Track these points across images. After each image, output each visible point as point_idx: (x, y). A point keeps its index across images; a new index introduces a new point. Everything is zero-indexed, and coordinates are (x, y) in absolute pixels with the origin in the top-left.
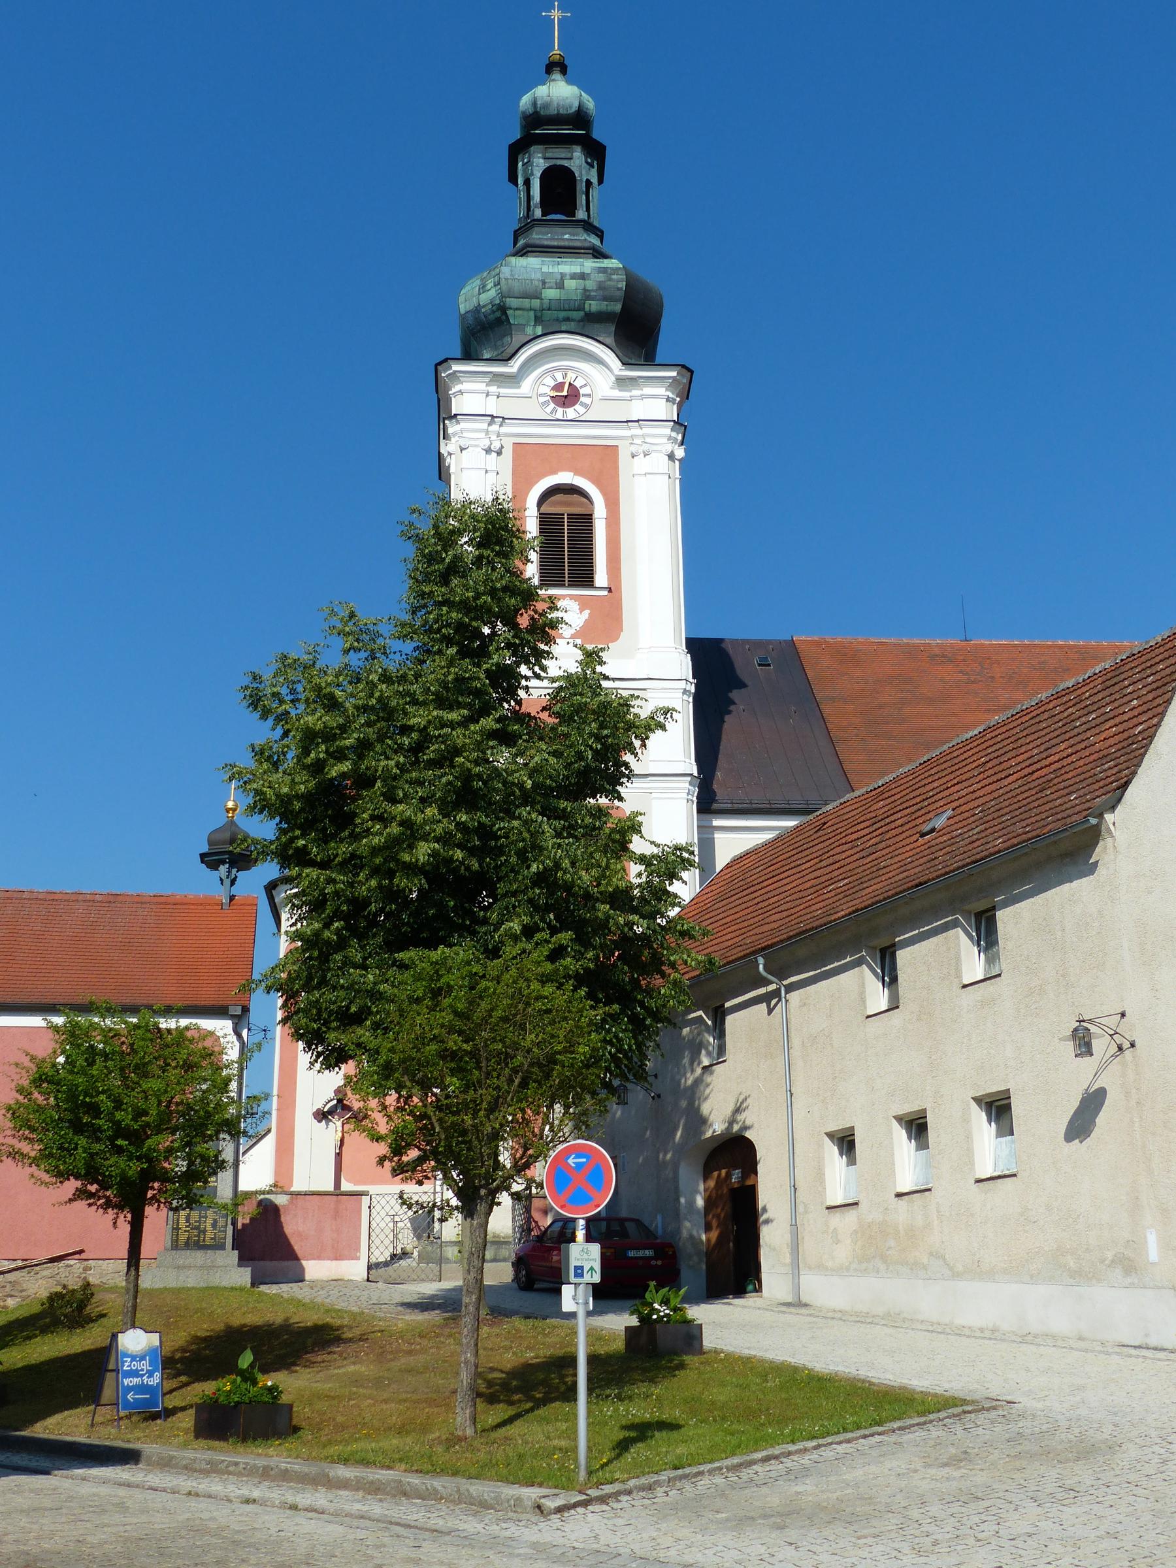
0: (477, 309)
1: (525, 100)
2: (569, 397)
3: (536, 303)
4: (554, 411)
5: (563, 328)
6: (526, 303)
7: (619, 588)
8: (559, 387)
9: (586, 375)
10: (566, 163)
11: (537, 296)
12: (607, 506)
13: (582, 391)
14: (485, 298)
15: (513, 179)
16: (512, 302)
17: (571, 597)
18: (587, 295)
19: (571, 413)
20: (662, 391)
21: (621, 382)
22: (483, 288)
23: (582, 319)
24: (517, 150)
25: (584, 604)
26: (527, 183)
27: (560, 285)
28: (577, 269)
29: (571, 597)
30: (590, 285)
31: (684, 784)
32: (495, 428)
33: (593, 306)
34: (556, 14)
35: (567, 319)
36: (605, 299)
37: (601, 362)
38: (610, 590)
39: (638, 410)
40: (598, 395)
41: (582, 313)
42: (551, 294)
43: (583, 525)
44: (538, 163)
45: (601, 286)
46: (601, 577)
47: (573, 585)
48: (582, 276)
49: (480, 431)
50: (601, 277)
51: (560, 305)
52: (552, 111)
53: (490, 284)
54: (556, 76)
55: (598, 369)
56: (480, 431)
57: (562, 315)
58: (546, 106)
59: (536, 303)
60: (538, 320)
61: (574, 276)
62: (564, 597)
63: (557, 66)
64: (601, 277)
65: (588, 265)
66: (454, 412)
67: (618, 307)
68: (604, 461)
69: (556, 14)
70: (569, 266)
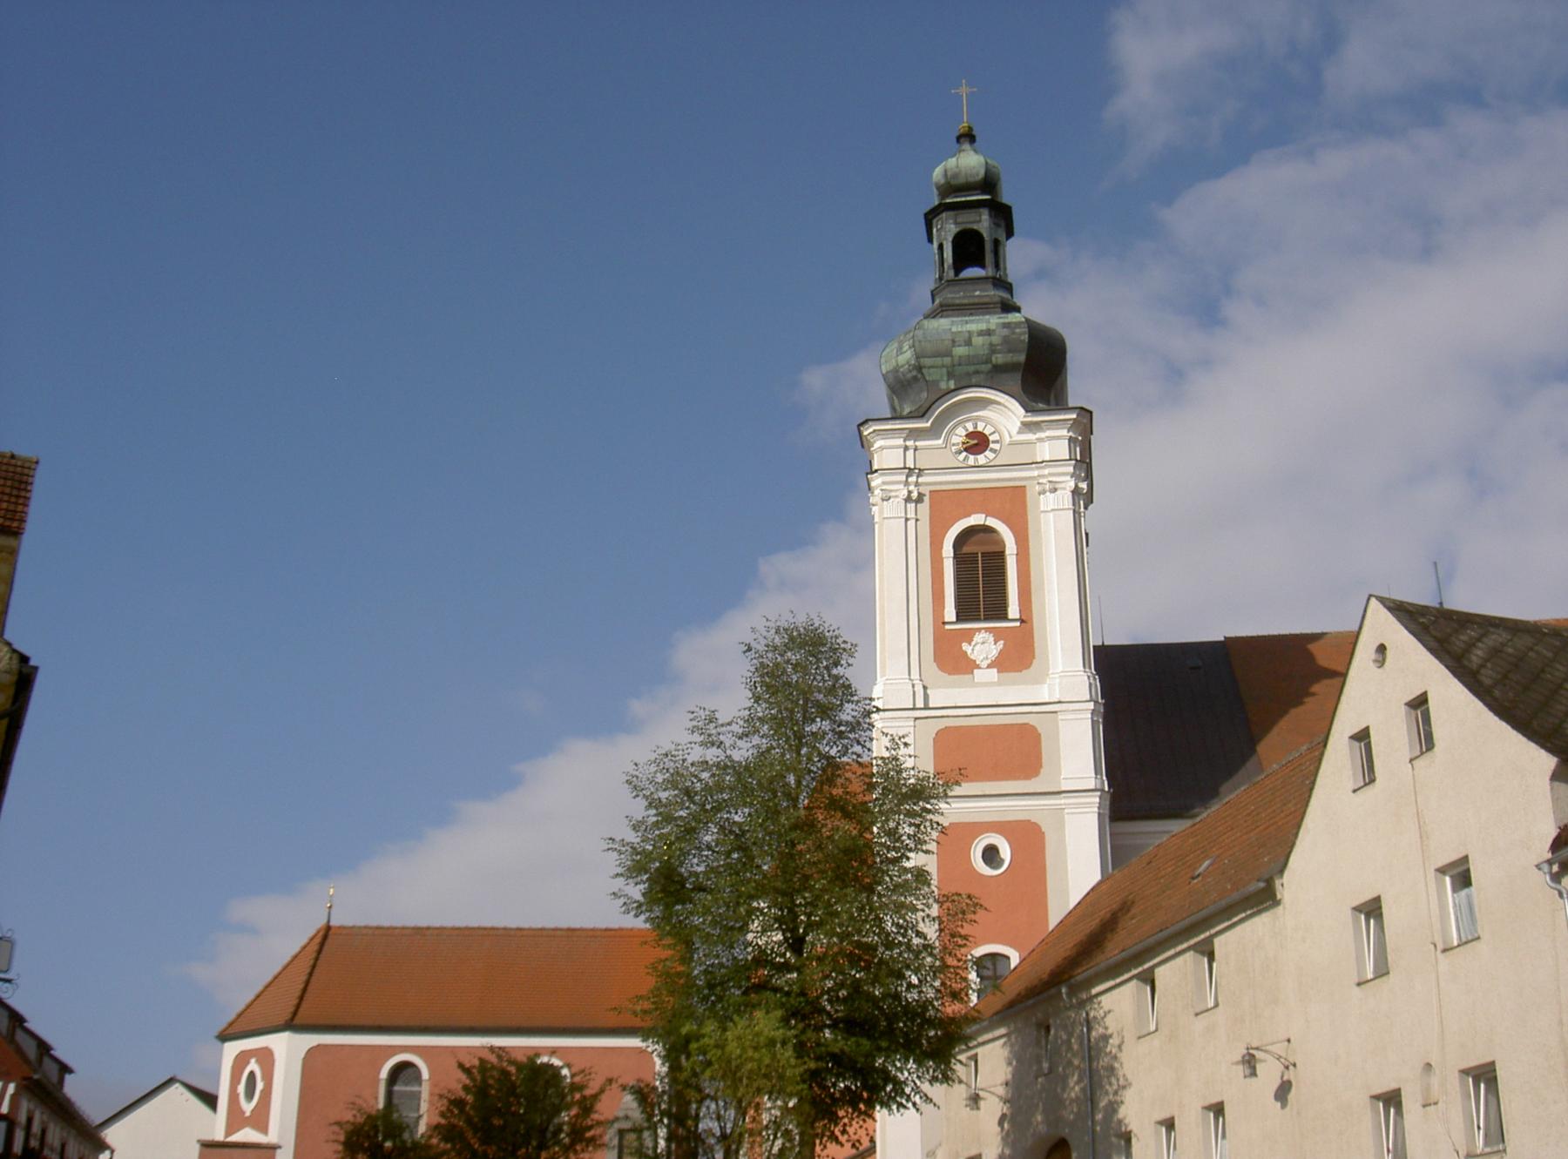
0: (896, 370)
1: (937, 174)
2: (978, 443)
3: (947, 360)
4: (966, 458)
5: (974, 381)
6: (938, 361)
7: (1031, 618)
8: (970, 435)
9: (987, 422)
10: (975, 227)
11: (949, 354)
12: (1017, 543)
13: (987, 432)
14: (902, 359)
15: (930, 240)
16: (927, 361)
17: (987, 629)
18: (993, 349)
19: (981, 459)
20: (1064, 432)
21: (1027, 427)
22: (900, 351)
23: (994, 375)
24: (930, 217)
25: (998, 635)
26: (941, 247)
27: (968, 343)
28: (983, 326)
29: (987, 629)
30: (995, 339)
31: (1095, 799)
32: (913, 479)
33: (999, 359)
34: (964, 91)
35: (977, 372)
36: (1010, 351)
37: (999, 403)
38: (1022, 621)
39: (1045, 451)
40: (1007, 440)
41: (989, 366)
42: (960, 351)
43: (996, 559)
44: (948, 229)
45: (1006, 340)
46: (1013, 610)
47: (987, 619)
48: (988, 333)
49: (898, 447)
50: (1006, 332)
51: (969, 360)
52: (961, 180)
53: (906, 347)
54: (966, 146)
55: (1004, 415)
56: (898, 447)
57: (972, 369)
58: (956, 176)
59: (947, 360)
60: (950, 375)
61: (981, 333)
62: (979, 630)
63: (968, 137)
64: (1006, 332)
65: (994, 321)
66: (875, 467)
67: (1022, 358)
68: (1013, 503)
69: (964, 91)
70: (975, 324)
